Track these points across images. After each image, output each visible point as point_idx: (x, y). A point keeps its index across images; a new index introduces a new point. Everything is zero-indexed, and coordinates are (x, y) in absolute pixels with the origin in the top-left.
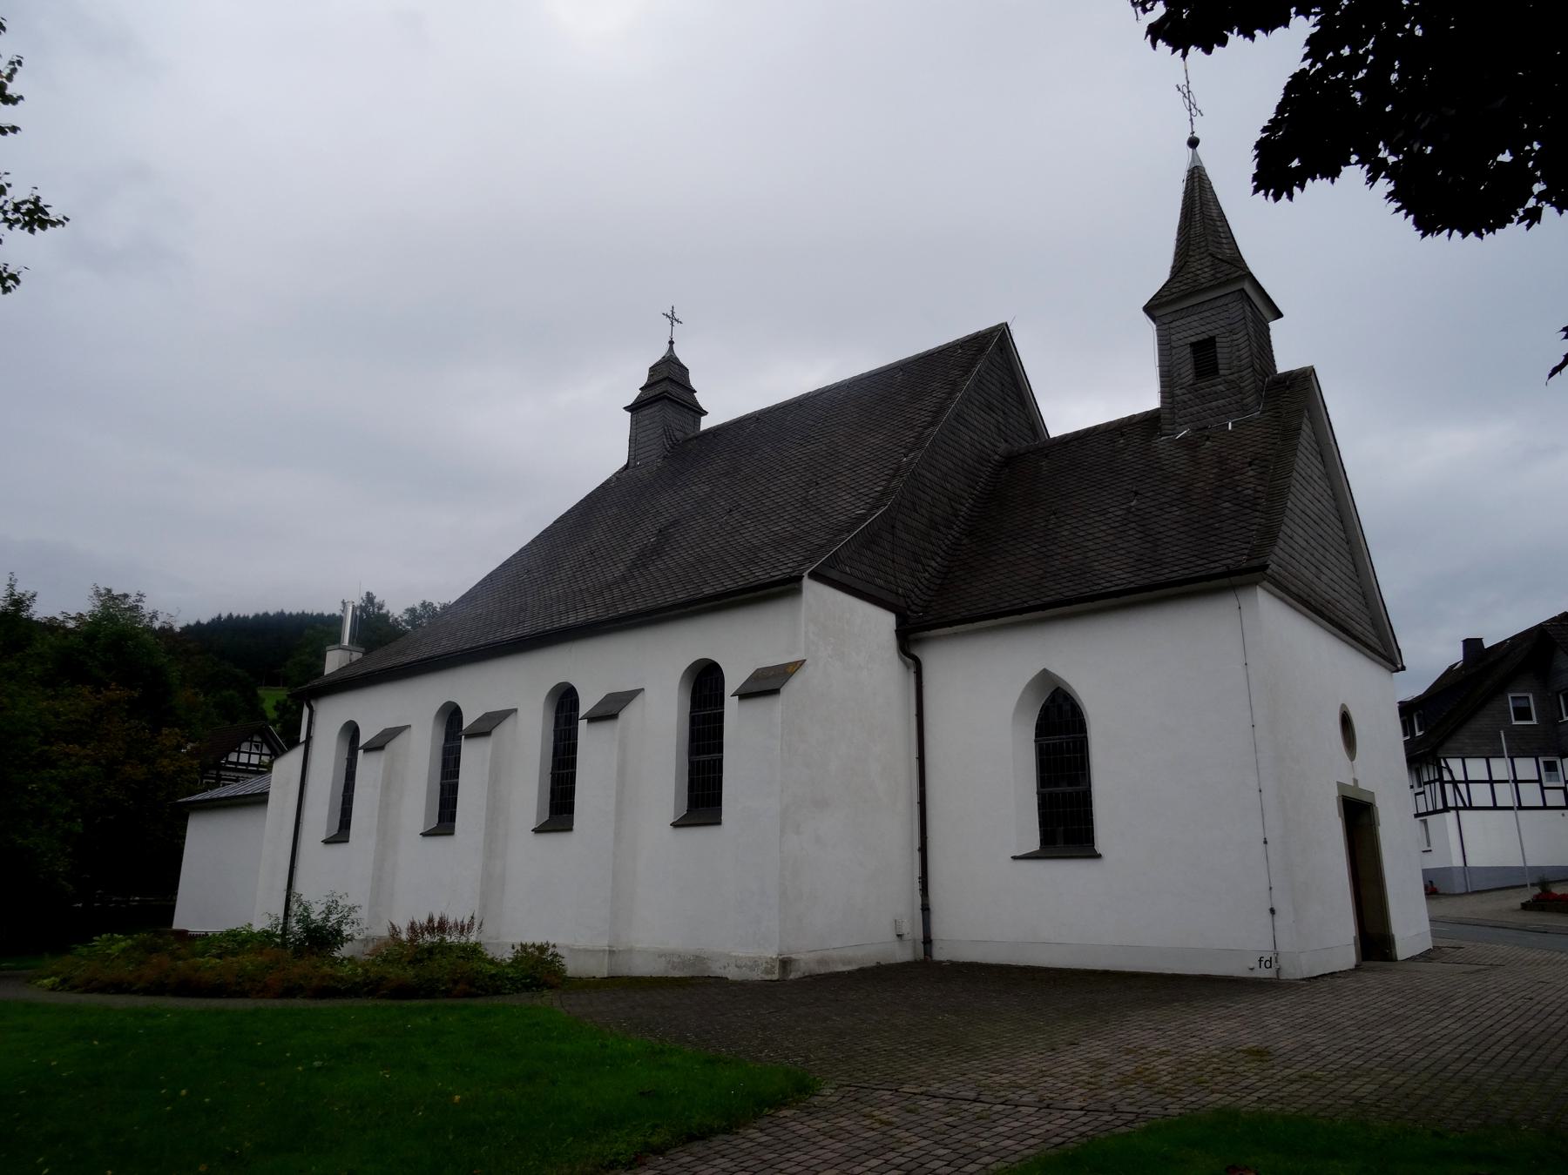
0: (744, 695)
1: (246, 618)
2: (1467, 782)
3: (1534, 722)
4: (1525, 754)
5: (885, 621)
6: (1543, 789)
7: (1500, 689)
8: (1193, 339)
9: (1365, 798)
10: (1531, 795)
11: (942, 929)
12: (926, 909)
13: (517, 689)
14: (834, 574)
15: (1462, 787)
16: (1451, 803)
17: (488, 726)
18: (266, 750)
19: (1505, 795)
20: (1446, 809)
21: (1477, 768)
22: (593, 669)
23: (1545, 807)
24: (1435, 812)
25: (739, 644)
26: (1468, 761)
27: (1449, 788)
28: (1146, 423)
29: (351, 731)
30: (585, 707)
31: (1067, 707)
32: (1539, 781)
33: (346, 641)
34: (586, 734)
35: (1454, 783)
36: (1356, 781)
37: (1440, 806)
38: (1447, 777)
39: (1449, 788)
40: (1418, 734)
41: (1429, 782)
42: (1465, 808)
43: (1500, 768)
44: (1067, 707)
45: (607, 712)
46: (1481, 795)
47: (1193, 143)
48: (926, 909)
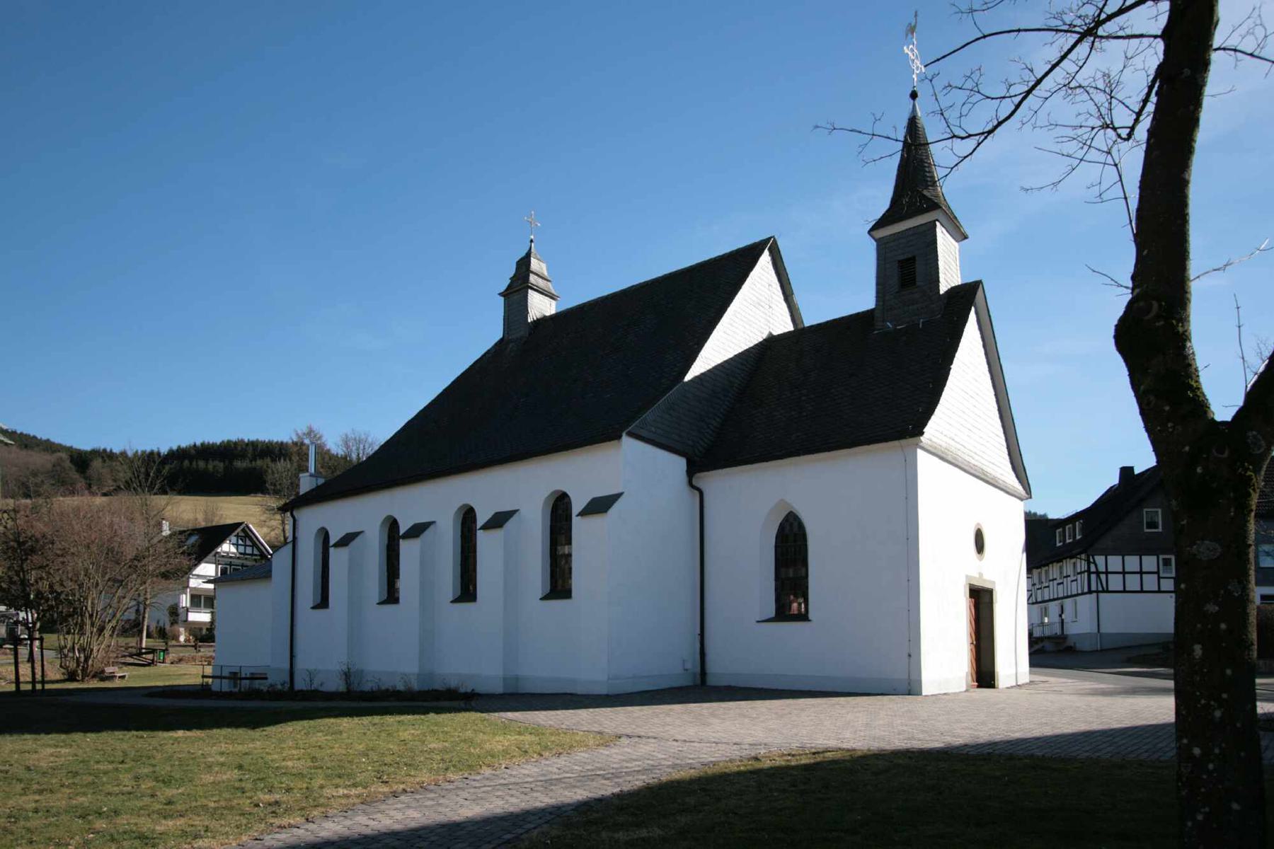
0: (584, 513)
1: (214, 445)
2: (1107, 573)
3: (1160, 530)
4: (1149, 552)
5: (679, 463)
6: (1159, 578)
7: (1140, 503)
8: (902, 258)
9: (988, 586)
10: (1150, 582)
11: (712, 667)
12: (702, 635)
13: (432, 502)
14: (644, 433)
15: (1103, 577)
16: (1093, 588)
17: (418, 530)
18: (248, 543)
19: (1133, 582)
20: (1090, 592)
21: (1115, 562)
22: (486, 489)
23: (1159, 591)
24: (1083, 594)
25: (579, 472)
26: (1127, 558)
27: (1093, 577)
28: (870, 312)
29: (324, 535)
30: (481, 521)
31: (796, 524)
32: (1158, 573)
33: (312, 470)
34: (482, 538)
35: (1098, 573)
36: (981, 574)
37: (1086, 590)
38: (1093, 569)
39: (1093, 577)
40: (1078, 537)
41: (1081, 573)
42: (1103, 591)
43: (1132, 562)
44: (796, 524)
45: (499, 520)
46: (1115, 582)
47: (914, 95)
48: (702, 635)
